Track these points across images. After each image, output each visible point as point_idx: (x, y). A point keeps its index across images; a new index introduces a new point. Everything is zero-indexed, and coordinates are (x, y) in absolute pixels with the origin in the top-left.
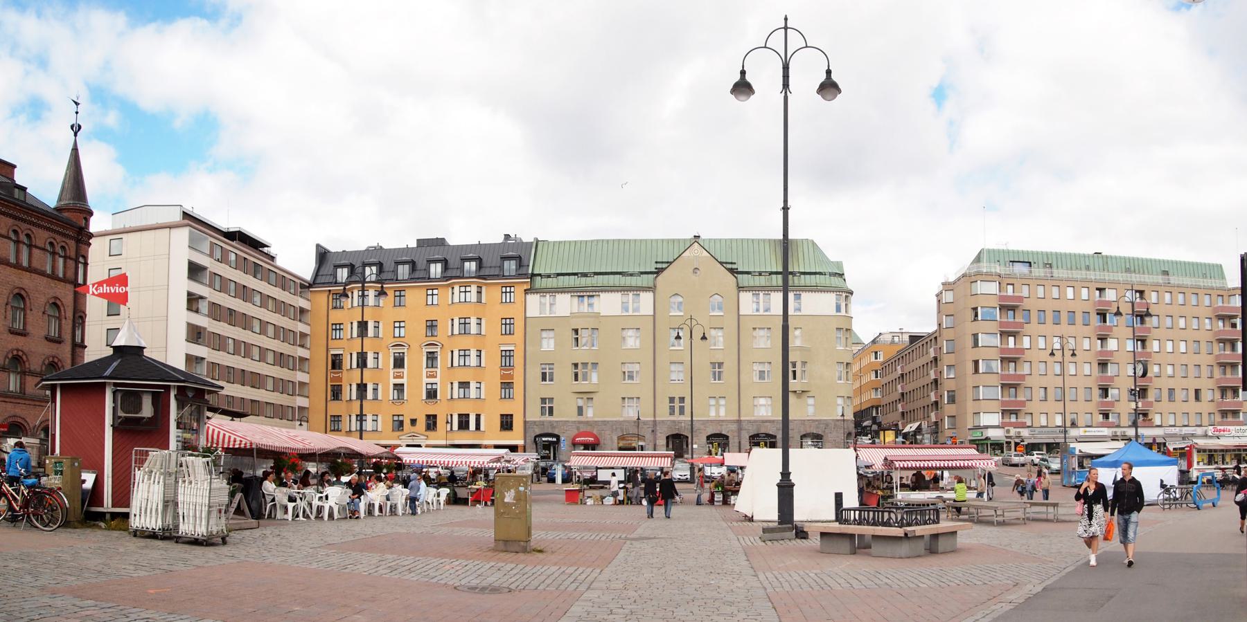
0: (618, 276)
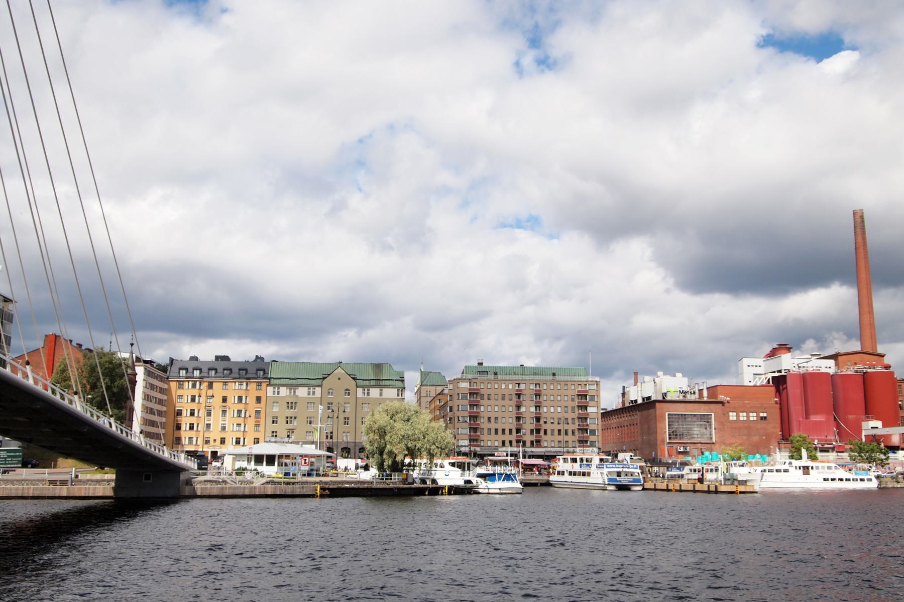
0: (306, 380)
